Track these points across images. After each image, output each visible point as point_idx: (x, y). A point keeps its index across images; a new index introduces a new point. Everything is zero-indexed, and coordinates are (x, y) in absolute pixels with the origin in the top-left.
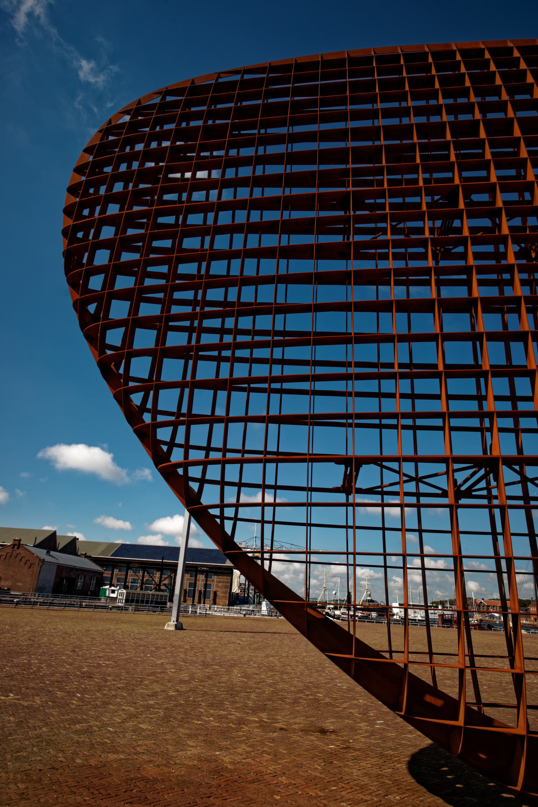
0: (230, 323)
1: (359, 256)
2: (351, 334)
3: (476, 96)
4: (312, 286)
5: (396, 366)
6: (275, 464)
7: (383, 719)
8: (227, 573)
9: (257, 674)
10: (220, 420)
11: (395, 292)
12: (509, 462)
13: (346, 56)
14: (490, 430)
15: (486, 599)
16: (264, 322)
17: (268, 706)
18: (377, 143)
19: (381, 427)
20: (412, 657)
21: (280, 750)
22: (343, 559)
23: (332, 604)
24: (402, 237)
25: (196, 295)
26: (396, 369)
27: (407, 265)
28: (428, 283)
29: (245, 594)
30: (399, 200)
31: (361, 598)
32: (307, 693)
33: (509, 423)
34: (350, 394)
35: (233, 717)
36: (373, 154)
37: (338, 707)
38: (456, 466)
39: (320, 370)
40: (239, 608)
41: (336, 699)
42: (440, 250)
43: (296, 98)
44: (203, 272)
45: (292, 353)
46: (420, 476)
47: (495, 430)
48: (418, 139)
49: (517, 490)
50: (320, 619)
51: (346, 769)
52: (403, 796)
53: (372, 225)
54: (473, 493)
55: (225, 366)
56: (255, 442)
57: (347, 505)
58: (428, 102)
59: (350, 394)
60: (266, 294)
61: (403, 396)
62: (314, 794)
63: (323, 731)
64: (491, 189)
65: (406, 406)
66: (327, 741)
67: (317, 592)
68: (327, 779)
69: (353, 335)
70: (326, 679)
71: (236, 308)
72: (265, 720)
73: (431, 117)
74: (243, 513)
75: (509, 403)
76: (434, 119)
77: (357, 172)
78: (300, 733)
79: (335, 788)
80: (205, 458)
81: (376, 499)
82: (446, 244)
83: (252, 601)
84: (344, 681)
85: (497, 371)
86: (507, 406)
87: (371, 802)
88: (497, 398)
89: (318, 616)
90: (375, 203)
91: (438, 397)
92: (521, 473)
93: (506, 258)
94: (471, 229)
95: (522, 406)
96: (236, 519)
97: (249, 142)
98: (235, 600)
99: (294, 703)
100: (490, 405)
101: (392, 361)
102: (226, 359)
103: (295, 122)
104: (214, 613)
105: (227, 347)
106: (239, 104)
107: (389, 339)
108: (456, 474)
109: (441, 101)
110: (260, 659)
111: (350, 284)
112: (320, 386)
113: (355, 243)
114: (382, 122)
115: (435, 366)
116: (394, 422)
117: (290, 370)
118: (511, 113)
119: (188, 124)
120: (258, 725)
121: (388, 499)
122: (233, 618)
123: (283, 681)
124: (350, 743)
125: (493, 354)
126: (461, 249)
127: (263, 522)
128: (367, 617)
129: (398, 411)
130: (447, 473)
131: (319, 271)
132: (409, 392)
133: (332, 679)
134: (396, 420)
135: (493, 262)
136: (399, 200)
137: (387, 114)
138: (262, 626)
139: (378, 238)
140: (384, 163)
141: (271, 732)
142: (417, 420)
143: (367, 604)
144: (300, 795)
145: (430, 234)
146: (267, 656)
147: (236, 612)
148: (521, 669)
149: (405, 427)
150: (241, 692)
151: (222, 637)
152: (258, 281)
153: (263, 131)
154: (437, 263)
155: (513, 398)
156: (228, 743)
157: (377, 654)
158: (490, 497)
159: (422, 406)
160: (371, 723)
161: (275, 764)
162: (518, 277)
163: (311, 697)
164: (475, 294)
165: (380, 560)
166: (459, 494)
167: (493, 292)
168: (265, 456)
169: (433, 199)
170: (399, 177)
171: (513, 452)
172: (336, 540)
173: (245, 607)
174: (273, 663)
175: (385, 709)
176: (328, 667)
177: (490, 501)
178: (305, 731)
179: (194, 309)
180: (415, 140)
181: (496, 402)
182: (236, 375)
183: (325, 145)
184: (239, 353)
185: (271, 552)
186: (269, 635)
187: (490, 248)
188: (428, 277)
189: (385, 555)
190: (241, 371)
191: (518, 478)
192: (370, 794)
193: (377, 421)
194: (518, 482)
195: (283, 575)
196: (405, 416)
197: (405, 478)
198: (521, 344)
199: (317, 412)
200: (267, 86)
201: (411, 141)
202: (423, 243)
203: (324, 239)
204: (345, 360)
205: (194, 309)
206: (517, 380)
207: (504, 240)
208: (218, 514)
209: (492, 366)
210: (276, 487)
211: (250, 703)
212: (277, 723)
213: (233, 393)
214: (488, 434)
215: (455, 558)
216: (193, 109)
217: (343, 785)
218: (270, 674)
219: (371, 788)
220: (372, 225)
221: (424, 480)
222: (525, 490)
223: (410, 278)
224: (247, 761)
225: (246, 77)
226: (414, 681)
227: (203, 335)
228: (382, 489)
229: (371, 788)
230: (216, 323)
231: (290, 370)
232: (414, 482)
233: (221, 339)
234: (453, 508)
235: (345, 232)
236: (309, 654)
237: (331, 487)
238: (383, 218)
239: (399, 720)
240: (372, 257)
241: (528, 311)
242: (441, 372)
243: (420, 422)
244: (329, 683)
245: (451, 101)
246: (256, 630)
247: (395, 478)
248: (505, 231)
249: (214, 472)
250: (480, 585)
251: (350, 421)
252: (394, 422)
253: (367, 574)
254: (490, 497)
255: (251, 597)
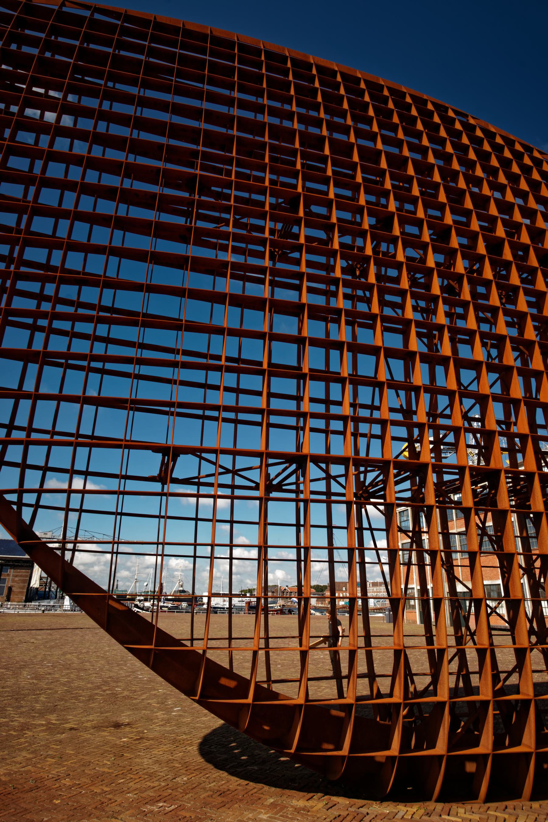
0: (50, 289)
1: (199, 243)
2: (182, 320)
3: (325, 113)
4: (146, 265)
5: (223, 359)
6: (88, 448)
7: (181, 706)
8: (27, 566)
9: (50, 674)
10: (27, 396)
11: (227, 285)
12: (316, 460)
13: (209, 32)
14: (303, 429)
15: (290, 586)
16: (90, 294)
17: (59, 707)
18: (230, 132)
19: (204, 418)
20: (212, 644)
21: (67, 751)
22: (152, 549)
23: (143, 596)
24: (244, 232)
25: (12, 251)
26: (223, 362)
27: (246, 261)
28: (262, 282)
29: (46, 588)
30: (246, 195)
31: (170, 589)
32: (105, 688)
33: (320, 424)
34: (175, 382)
35: (16, 724)
36: (225, 143)
37: (136, 699)
38: (271, 461)
39: (148, 354)
40: (37, 604)
41: (135, 691)
42: (278, 252)
43: (151, 60)
44: (23, 226)
45: (119, 332)
46: (236, 468)
47: (307, 429)
48: (269, 138)
49: (321, 486)
50: (122, 611)
51: (137, 760)
52: (189, 777)
53: (217, 214)
54: (284, 487)
55: (40, 337)
56: (67, 424)
57: (161, 494)
58: (282, 105)
59: (175, 382)
60: (96, 264)
61: (227, 389)
62: (99, 791)
63: (117, 726)
64: (328, 204)
65: (229, 399)
66: (120, 735)
67: (128, 584)
68: (116, 773)
70: (127, 672)
71: (58, 274)
72: (54, 722)
73: (284, 121)
74: (46, 499)
75: (323, 406)
76: (286, 124)
77: (206, 156)
78: (92, 731)
79: (122, 781)
80: (6, 436)
81: (192, 489)
82: (284, 248)
83: (53, 596)
84: (145, 673)
85: (315, 375)
86: (320, 408)
87: (158, 788)
88: (312, 400)
89: (120, 608)
90: (222, 192)
91: (260, 394)
92: (326, 471)
93: (334, 271)
94: (307, 238)
95: (334, 410)
96: (37, 506)
97: (93, 92)
98: (32, 596)
99: (89, 700)
100: (306, 406)
101: (220, 354)
102: (41, 329)
103: (146, 85)
104: (6, 611)
105: (44, 315)
106: (85, 45)
107: (220, 331)
108: (270, 469)
109: (294, 108)
110: (56, 657)
111: (187, 270)
112: (145, 370)
113: (197, 229)
114: (236, 112)
115: (260, 364)
116: (215, 414)
117: (114, 350)
118: (352, 139)
119: (19, 47)
120: (45, 728)
121: (204, 490)
122: (30, 615)
123: (79, 678)
124: (144, 733)
125: (314, 359)
126: (296, 255)
127: (67, 510)
128: (177, 608)
129: (221, 404)
130: (260, 467)
131: (157, 250)
133: (133, 672)
134: (218, 412)
135: (323, 273)
136: (246, 195)
137: (243, 105)
138: (62, 621)
139: (221, 229)
140: (234, 154)
141: (58, 733)
142: (239, 414)
143: (179, 594)
144: (83, 794)
146: (64, 654)
147: (33, 609)
148: (306, 646)
149: (225, 420)
150: (28, 695)
151: (13, 637)
152: (88, 249)
153: (110, 84)
154: (274, 264)
155: (327, 402)
156: (6, 752)
157: (178, 643)
158: (297, 492)
159: (246, 401)
160: (169, 711)
161: (59, 766)
162: (341, 290)
163: (108, 692)
164: (304, 300)
165: (190, 550)
166: (270, 487)
167: (320, 300)
168: (77, 439)
169: (277, 201)
170: (248, 172)
171: (321, 451)
172: (148, 530)
173: (45, 603)
174: (70, 660)
175: (183, 696)
176: (131, 660)
177: (297, 496)
178: (98, 728)
179: (8, 267)
180: (267, 139)
181: (390, 413)
182: (50, 348)
183: (178, 120)
184: (57, 324)
185: (75, 542)
186: (69, 631)
187: (322, 260)
188: (263, 276)
189: (195, 545)
190: (58, 344)
191: (323, 475)
192: (158, 780)
193: (200, 412)
194: (323, 479)
195: (93, 567)
196: (227, 409)
197: (221, 470)
198: (338, 352)
199: (140, 397)
200: (120, 35)
201: (262, 139)
202: (262, 242)
203: (167, 218)
204: (174, 347)
205: (8, 267)
206: (332, 385)
207: (333, 254)
208: (16, 500)
209: (310, 370)
210: (86, 474)
211: (38, 706)
212: (67, 723)
213: (46, 368)
214: (302, 432)
215: (260, 547)
216: (27, 32)
217: (132, 776)
218: (65, 672)
219: (160, 774)
220: (217, 214)
222: (328, 486)
224: (26, 769)
225: (97, 16)
226: (211, 664)
227: (15, 298)
229: (160, 774)
230: (34, 287)
231: (114, 350)
232: (230, 475)
233: (39, 306)
234: (264, 501)
235: (187, 215)
236: (112, 648)
237: (147, 475)
238: (227, 210)
239: (196, 705)
240: (213, 246)
241: (347, 323)
242: (265, 370)
243: (242, 416)
244: (129, 676)
245: (303, 111)
246: (54, 627)
247: (211, 469)
248: (336, 246)
249: (37, 455)
251: (172, 409)
252: (215, 414)
253: (181, 565)
254: (297, 492)
255: (52, 592)
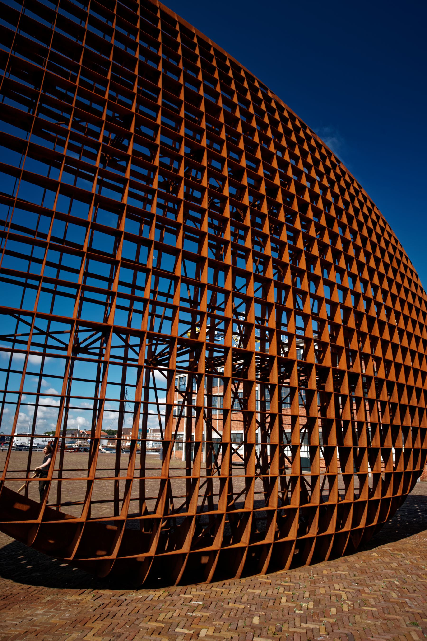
1: (38, 132)
12: (118, 331)
19: (25, 285)
20: (9, 475)
33: (126, 303)
38: (81, 328)
42: (109, 158)
54: (89, 351)
58: (129, 35)
65: (52, 273)
69: (16, 199)
75: (130, 289)
77: (53, 56)
85: (126, 263)
86: (128, 291)
92: (126, 341)
100: (115, 287)
115: (81, 247)
116: (36, 283)
121: (18, 346)
132: (58, 263)
135: (144, 183)
142: (58, 286)
145: (104, 141)
148: (92, 477)
155: (134, 286)
159: (65, 276)
164: (125, 201)
166: (77, 349)
177: (100, 358)
188: (93, 175)
191: (123, 344)
193: (23, 280)
194: (123, 347)
197: (35, 331)
221: (53, 335)
222: (126, 353)
223: (76, 169)
228: (15, 338)
234: (71, 361)
235: (31, 105)
240: (52, 139)
243: (60, 288)
250: (86, 420)
252: (36, 283)
